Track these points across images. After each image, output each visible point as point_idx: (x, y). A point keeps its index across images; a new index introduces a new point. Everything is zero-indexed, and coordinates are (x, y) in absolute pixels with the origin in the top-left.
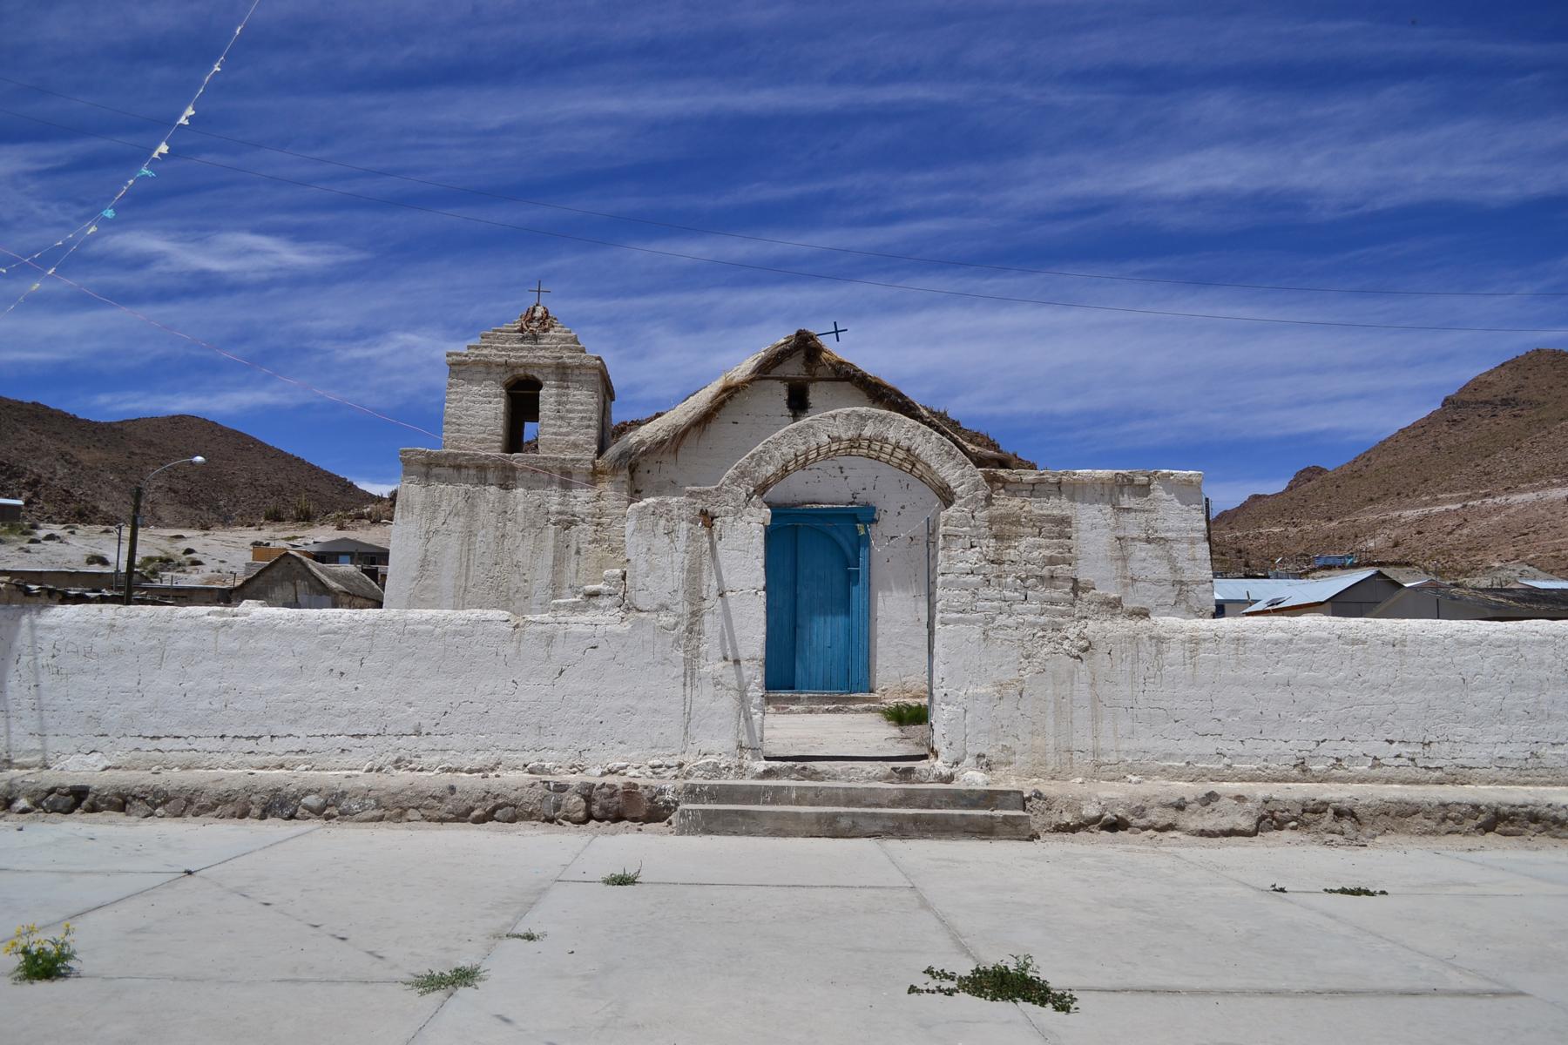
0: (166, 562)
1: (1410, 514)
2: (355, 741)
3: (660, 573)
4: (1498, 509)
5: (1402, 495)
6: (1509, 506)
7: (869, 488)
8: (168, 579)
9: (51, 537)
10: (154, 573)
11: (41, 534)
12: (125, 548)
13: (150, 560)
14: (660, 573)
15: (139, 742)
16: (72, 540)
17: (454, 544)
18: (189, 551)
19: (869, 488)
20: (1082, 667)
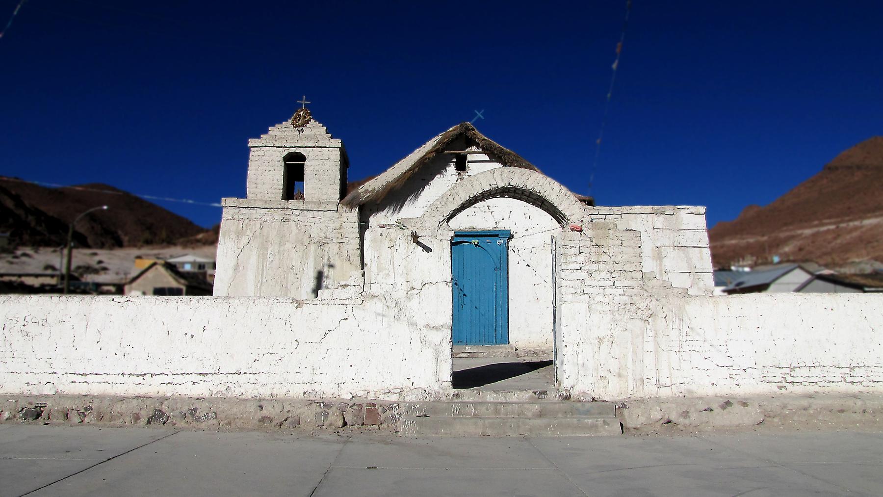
0: (89, 269)
1: (808, 232)
2: (202, 377)
3: (384, 272)
4: (856, 228)
5: (805, 220)
6: (861, 227)
7: (506, 218)
8: (90, 278)
9: (25, 255)
10: (82, 275)
11: (19, 252)
12: (65, 261)
13: (79, 268)
14: (387, 272)
15: (75, 377)
16: (36, 256)
17: (254, 260)
18: (100, 262)
19: (506, 218)
20: (649, 327)
